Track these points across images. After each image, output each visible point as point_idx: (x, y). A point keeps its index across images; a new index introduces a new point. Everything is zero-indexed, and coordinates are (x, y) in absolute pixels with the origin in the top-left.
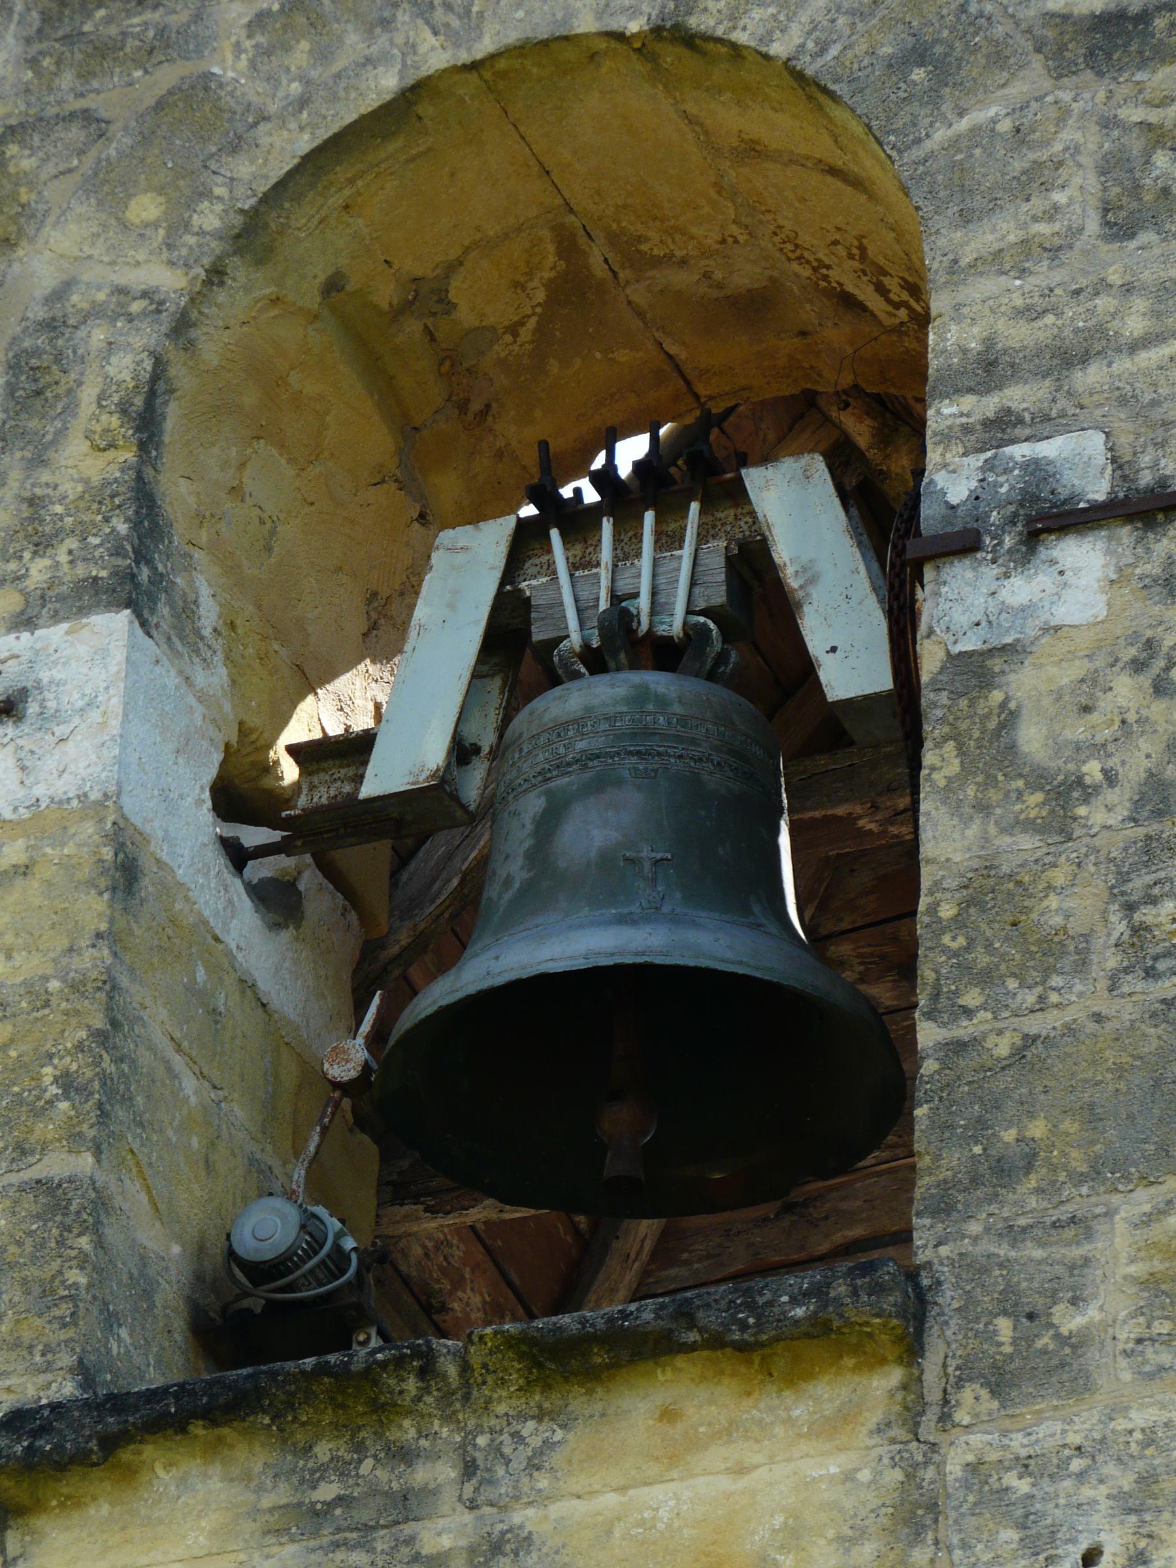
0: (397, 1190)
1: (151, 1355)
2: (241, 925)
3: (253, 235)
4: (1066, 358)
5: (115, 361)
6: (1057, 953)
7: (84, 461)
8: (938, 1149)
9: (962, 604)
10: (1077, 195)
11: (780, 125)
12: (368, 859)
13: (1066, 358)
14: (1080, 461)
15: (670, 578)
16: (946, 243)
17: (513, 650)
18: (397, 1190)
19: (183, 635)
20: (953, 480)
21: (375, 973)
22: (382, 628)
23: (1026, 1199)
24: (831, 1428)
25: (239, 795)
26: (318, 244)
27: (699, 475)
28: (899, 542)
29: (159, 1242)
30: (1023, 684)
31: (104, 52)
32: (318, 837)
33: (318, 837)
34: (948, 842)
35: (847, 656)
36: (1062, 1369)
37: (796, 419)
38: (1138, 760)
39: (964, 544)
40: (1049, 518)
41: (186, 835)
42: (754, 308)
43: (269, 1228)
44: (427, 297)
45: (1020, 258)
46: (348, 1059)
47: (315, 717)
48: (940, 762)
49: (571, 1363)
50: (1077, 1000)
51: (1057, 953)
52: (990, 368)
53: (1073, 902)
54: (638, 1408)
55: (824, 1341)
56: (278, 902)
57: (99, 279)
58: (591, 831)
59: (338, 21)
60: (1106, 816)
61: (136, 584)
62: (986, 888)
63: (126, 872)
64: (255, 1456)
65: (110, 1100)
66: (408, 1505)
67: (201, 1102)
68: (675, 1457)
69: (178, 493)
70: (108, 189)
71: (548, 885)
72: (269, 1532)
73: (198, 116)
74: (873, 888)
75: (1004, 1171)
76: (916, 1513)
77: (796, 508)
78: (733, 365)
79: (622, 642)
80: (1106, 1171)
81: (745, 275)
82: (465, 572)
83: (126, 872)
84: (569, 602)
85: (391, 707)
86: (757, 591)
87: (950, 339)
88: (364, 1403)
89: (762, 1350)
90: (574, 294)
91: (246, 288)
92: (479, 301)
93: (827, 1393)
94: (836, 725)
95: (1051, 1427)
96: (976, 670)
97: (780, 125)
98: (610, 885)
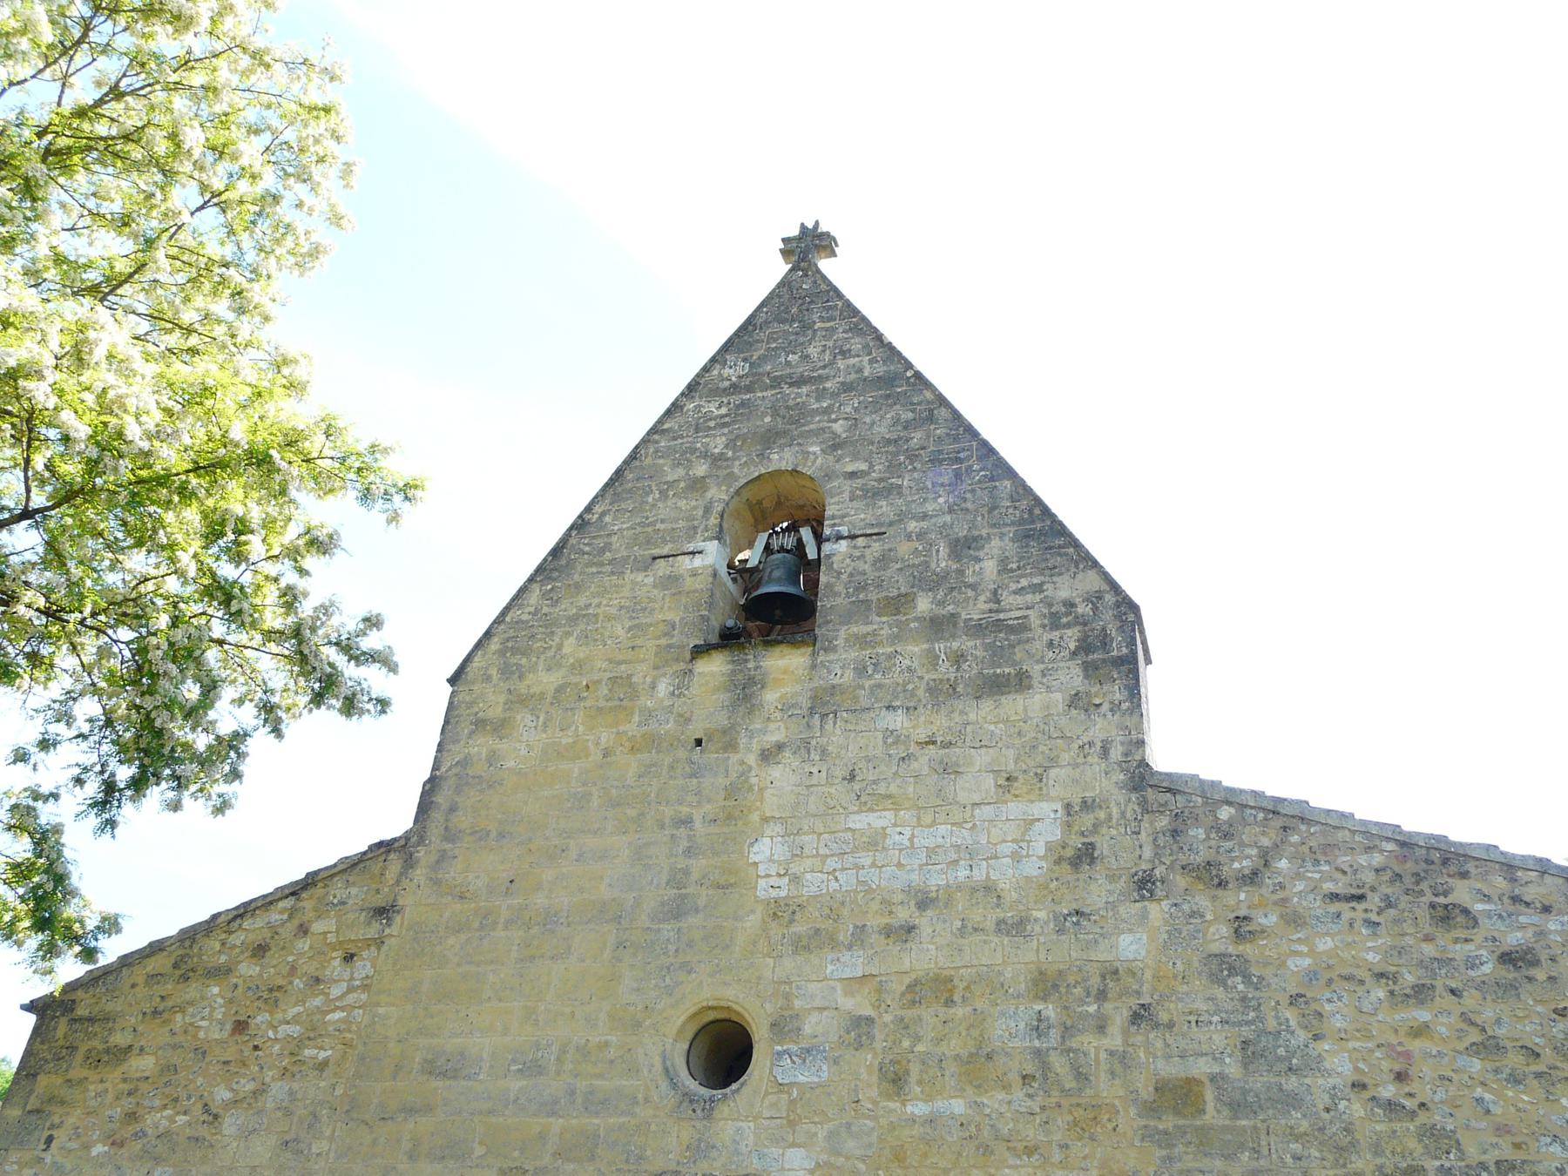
0: (747, 619)
1: (714, 639)
2: (730, 583)
3: (738, 492)
4: (843, 516)
5: (719, 508)
6: (838, 594)
7: (713, 520)
8: (819, 618)
9: (827, 548)
10: (846, 495)
11: (808, 484)
12: (746, 576)
13: (843, 516)
14: (844, 530)
15: (789, 542)
16: (829, 500)
17: (768, 549)
18: (747, 619)
19: (725, 544)
20: (827, 531)
21: (746, 591)
22: (750, 545)
23: (830, 626)
24: (803, 655)
25: (730, 566)
26: (746, 495)
27: (793, 528)
28: (819, 539)
29: (716, 624)
30: (834, 558)
31: (720, 467)
32: (741, 573)
33: (741, 573)
34: (823, 579)
35: (811, 554)
36: (834, 649)
37: (807, 522)
38: (849, 570)
39: (828, 540)
40: (839, 537)
41: (723, 571)
42: (802, 507)
43: (730, 623)
44: (760, 503)
45: (838, 503)
46: (742, 602)
47: (741, 556)
48: (823, 568)
49: (769, 644)
50: (839, 601)
51: (838, 594)
52: (833, 517)
53: (839, 588)
54: (777, 650)
55: (803, 643)
56: (734, 580)
57: (716, 497)
58: (776, 574)
59: (324, 968)
60: (844, 577)
61: (719, 537)
62: (828, 585)
63: (715, 575)
64: (726, 653)
65: (711, 605)
66: (746, 661)
67: (722, 605)
68: (782, 657)
69: (725, 525)
70: (719, 485)
71: (770, 581)
72: (1012, 630)
73: (731, 476)
74: (813, 584)
75: (828, 622)
76: (814, 667)
77: (806, 533)
78: (799, 515)
79: (782, 549)
80: (841, 623)
81: (801, 502)
82: (762, 540)
83: (715, 575)
84: (775, 545)
85: (750, 556)
86: (800, 544)
87: (828, 513)
88: (741, 647)
89: (794, 644)
90: (779, 503)
91: (736, 499)
92: (766, 504)
93: (803, 650)
94: (809, 562)
95: (832, 657)
96: (828, 557)
97: (808, 484)
98: (778, 581)
